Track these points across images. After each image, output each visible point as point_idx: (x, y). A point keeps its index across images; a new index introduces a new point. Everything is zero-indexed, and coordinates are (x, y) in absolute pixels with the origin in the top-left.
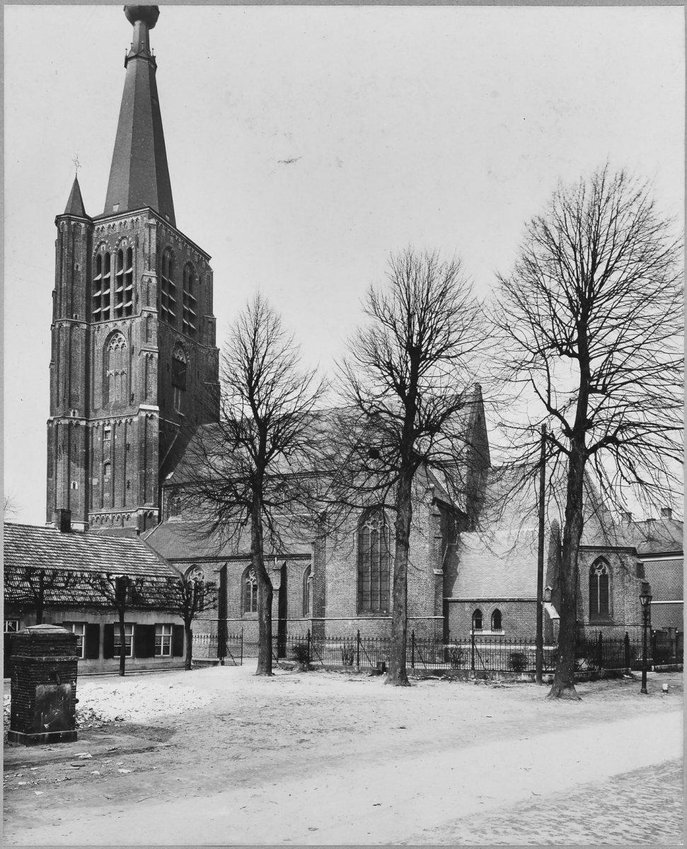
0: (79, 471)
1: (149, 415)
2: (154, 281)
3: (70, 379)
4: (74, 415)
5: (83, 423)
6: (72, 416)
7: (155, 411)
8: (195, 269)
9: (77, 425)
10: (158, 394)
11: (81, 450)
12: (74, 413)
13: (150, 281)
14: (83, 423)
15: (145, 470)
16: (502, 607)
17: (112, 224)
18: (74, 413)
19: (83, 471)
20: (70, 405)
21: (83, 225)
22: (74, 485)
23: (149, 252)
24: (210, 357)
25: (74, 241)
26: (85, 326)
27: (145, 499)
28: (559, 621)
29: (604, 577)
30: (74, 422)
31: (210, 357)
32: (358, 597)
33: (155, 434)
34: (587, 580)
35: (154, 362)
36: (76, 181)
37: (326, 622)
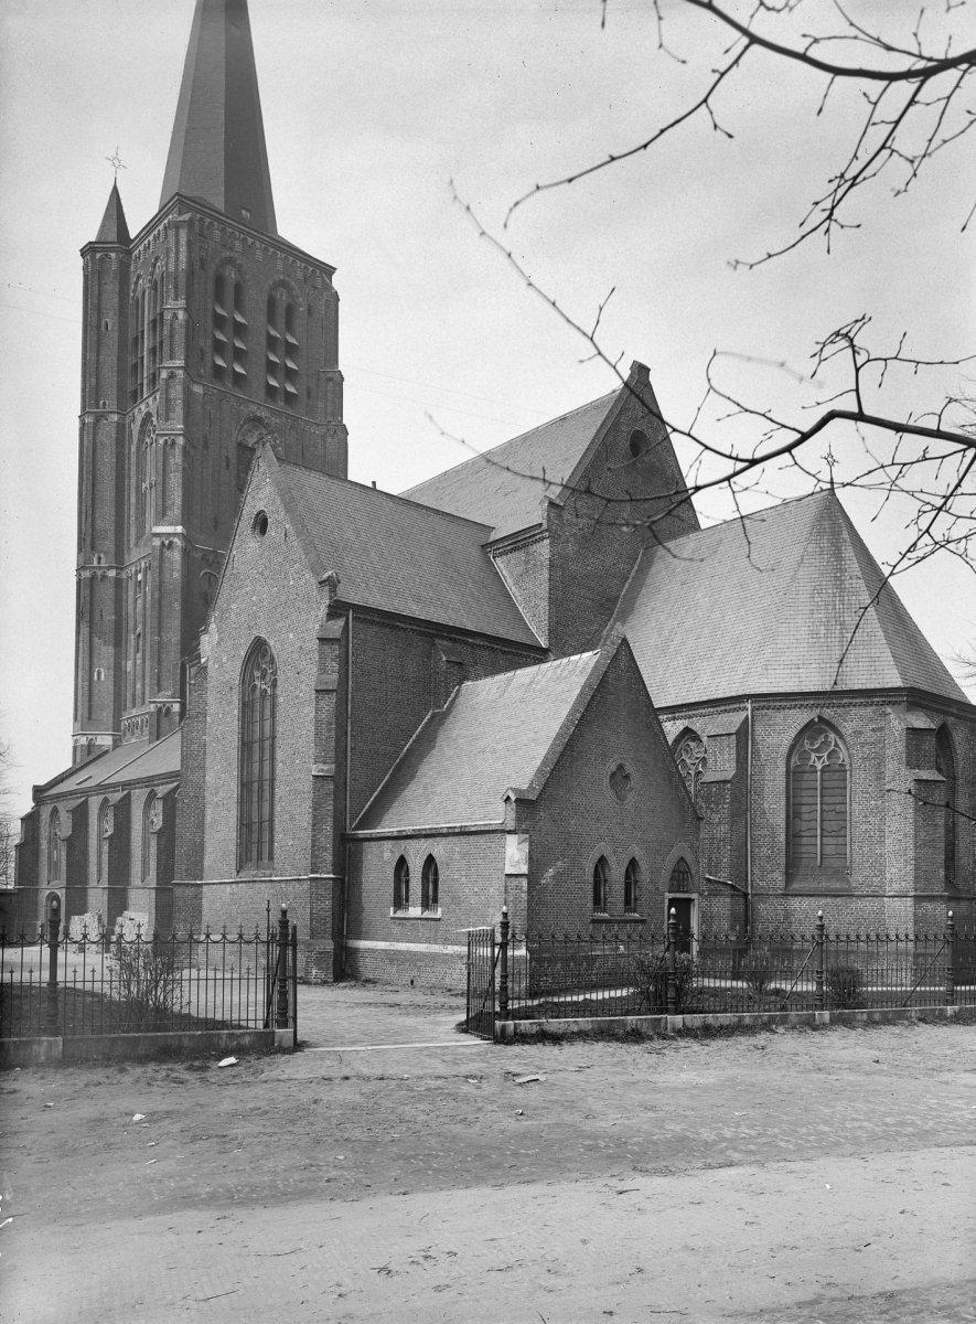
0: (106, 651)
1: (167, 542)
2: (181, 315)
3: (93, 504)
4: (99, 563)
5: (112, 573)
6: (95, 564)
7: (175, 535)
8: (297, 292)
9: (104, 577)
10: (183, 505)
11: (110, 617)
12: (100, 558)
13: (175, 316)
14: (112, 573)
15: (159, 636)
16: (439, 849)
17: (146, 242)
18: (100, 558)
19: (111, 650)
20: (93, 548)
21: (113, 255)
22: (99, 673)
23: (176, 269)
24: (329, 439)
25: (100, 285)
26: (115, 418)
27: (159, 685)
28: (524, 883)
29: (837, 772)
30: (99, 573)
31: (329, 439)
32: (240, 836)
33: (175, 574)
34: (781, 783)
35: (178, 451)
36: (115, 191)
37: (205, 889)
